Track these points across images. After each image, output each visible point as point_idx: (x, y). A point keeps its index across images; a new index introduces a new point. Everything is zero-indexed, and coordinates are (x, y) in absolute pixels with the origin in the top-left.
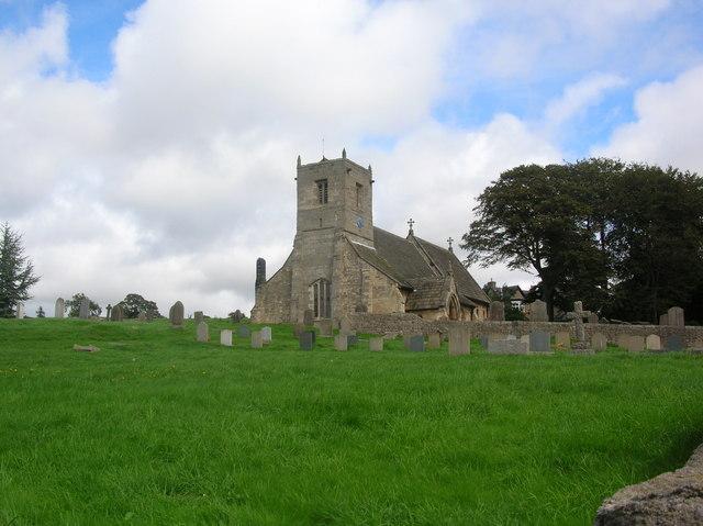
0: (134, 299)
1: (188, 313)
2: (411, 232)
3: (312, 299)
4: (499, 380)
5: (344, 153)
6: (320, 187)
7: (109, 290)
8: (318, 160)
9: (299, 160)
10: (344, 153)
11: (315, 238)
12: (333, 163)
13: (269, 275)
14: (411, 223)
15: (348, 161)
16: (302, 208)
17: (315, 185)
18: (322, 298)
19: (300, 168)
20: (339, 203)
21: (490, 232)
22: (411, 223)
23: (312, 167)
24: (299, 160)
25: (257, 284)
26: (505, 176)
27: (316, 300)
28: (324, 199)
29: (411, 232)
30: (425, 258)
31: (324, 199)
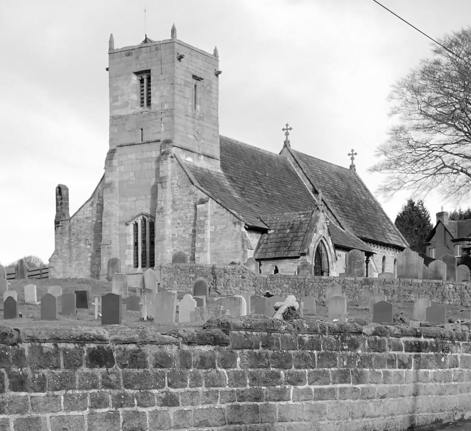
1: (439, 419)
2: (286, 144)
3: (132, 243)
5: (173, 31)
6: (142, 81)
7: (379, 301)
8: (138, 41)
9: (111, 42)
10: (173, 31)
11: (133, 156)
14: (287, 130)
15: (180, 44)
16: (118, 112)
17: (135, 79)
18: (144, 242)
19: (112, 52)
20: (166, 107)
22: (287, 130)
23: (129, 52)
24: (111, 42)
25: (57, 223)
26: (108, 154)
27: (136, 244)
29: (286, 144)
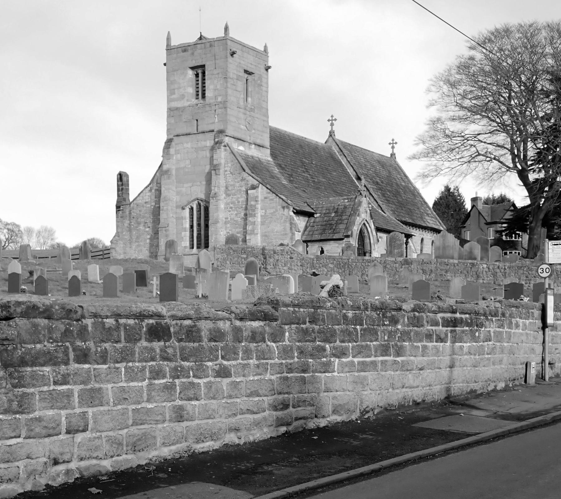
0: (241, 321)
2: (331, 134)
3: (188, 226)
4: (515, 365)
5: (226, 29)
6: (197, 75)
7: (418, 280)
9: (168, 39)
10: (226, 29)
11: (189, 145)
12: (212, 43)
13: (133, 192)
15: (233, 41)
16: (175, 104)
17: (191, 74)
18: (199, 225)
19: (169, 49)
20: (220, 99)
21: (494, 117)
22: (332, 121)
23: (185, 48)
24: (168, 39)
25: (118, 207)
26: (165, 143)
27: (192, 227)
28: (201, 93)
29: (331, 134)
30: (350, 171)
31: (201, 93)
